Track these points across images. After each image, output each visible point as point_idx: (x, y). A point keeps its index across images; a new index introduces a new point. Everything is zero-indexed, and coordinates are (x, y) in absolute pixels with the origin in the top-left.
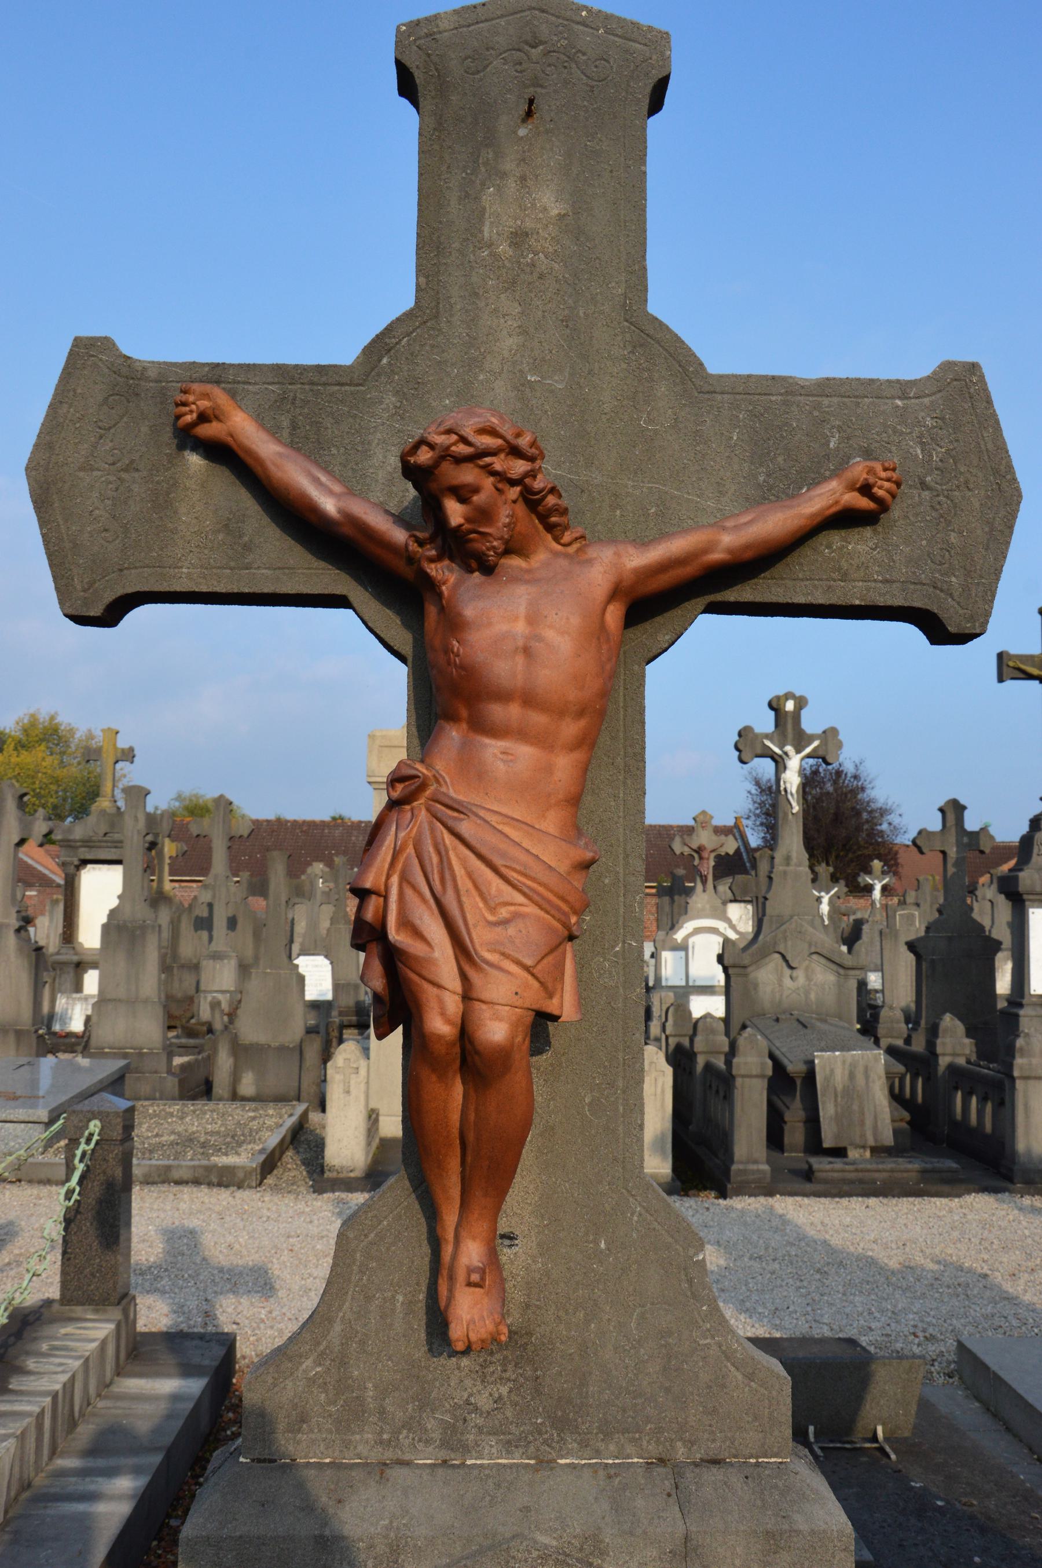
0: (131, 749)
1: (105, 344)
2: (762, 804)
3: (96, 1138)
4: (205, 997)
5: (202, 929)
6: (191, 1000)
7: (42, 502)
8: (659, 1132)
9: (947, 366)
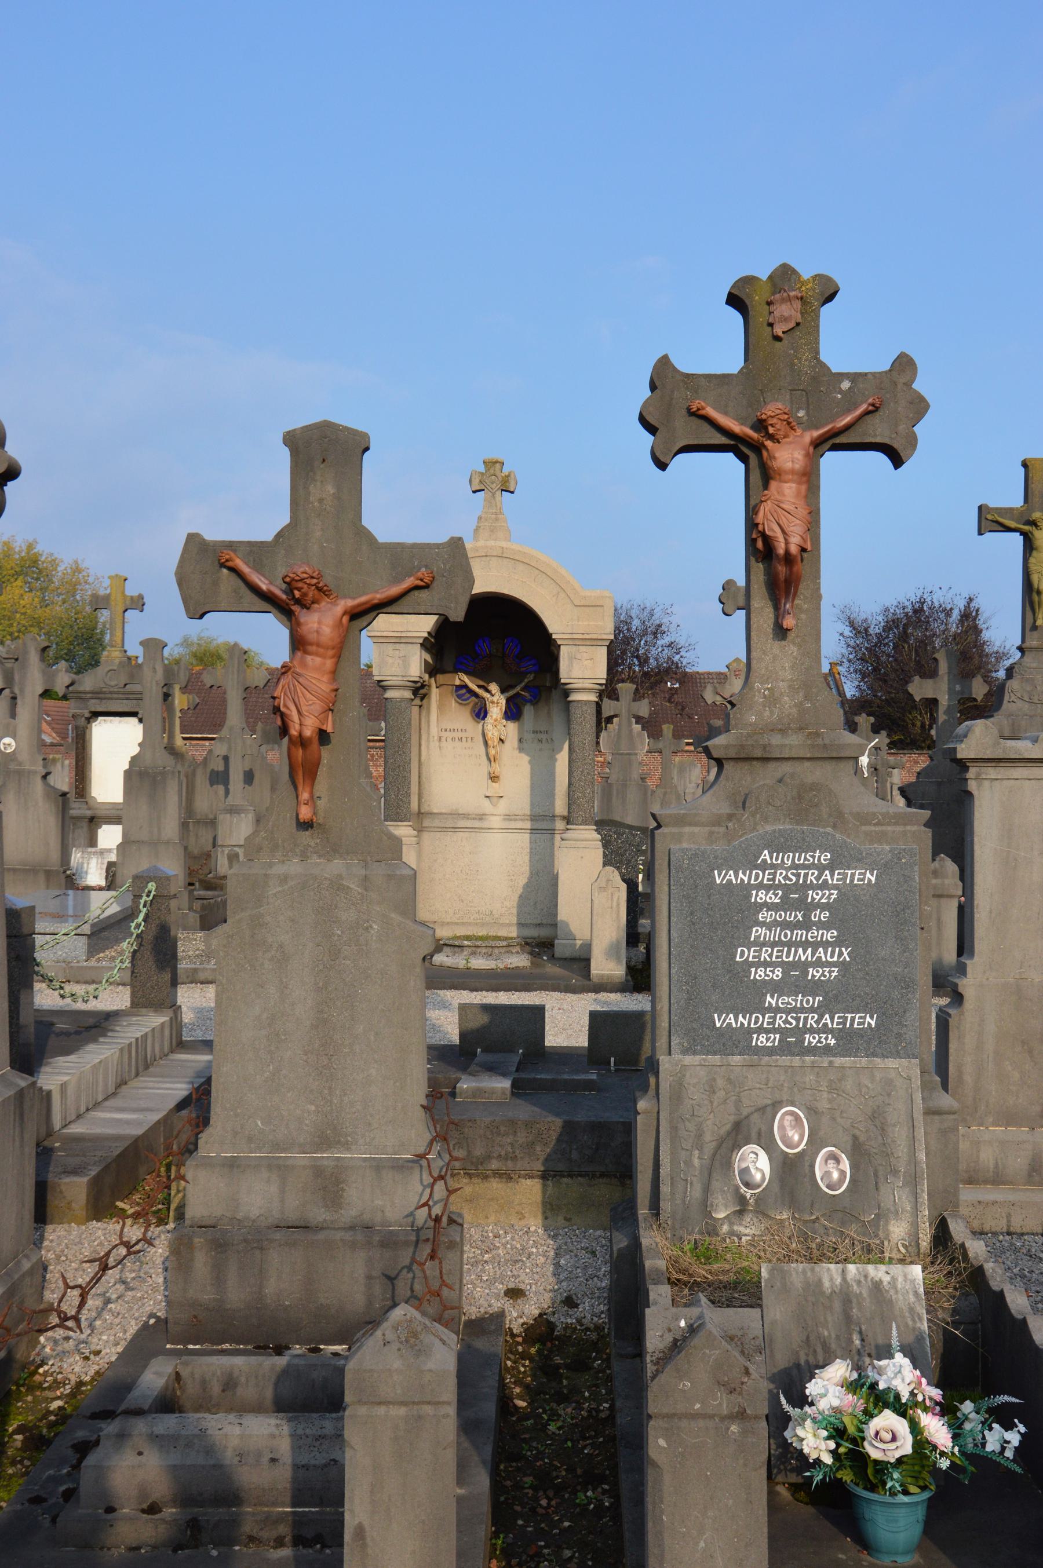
0: (141, 597)
1: (197, 535)
2: (856, 648)
3: (153, 893)
4: (223, 851)
5: (218, 783)
6: (208, 856)
7: (180, 584)
8: (614, 940)
9: (452, 538)
